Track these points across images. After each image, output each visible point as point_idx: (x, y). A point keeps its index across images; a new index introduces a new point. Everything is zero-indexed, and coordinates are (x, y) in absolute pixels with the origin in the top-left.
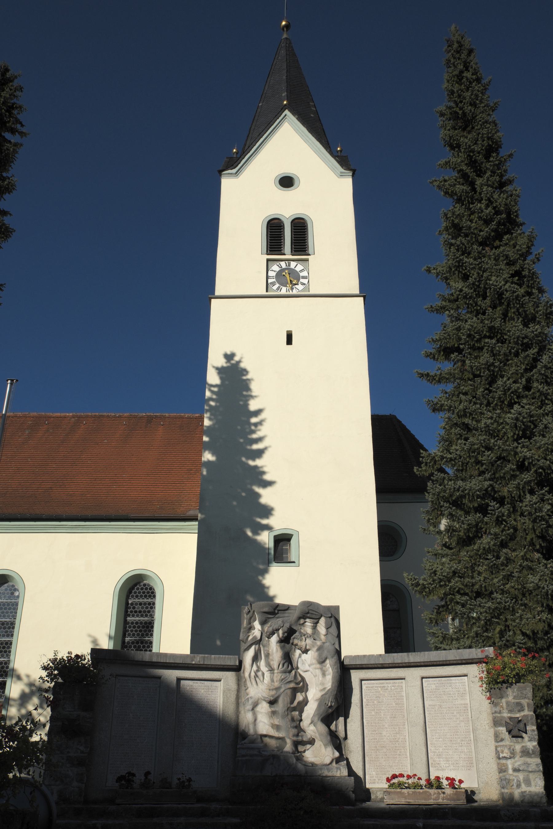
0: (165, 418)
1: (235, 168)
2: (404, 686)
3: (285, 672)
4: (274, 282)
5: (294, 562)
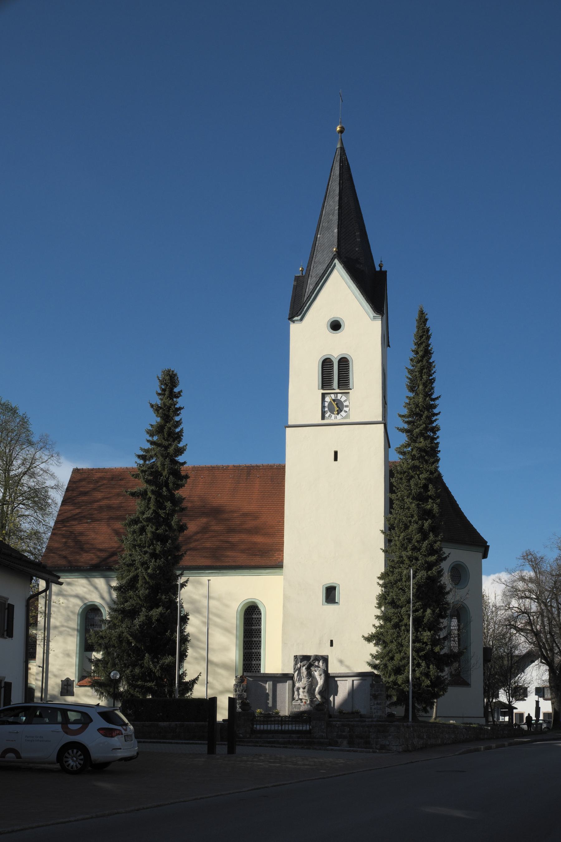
0: (260, 469)
1: (299, 315)
4: (330, 415)
5: (338, 603)
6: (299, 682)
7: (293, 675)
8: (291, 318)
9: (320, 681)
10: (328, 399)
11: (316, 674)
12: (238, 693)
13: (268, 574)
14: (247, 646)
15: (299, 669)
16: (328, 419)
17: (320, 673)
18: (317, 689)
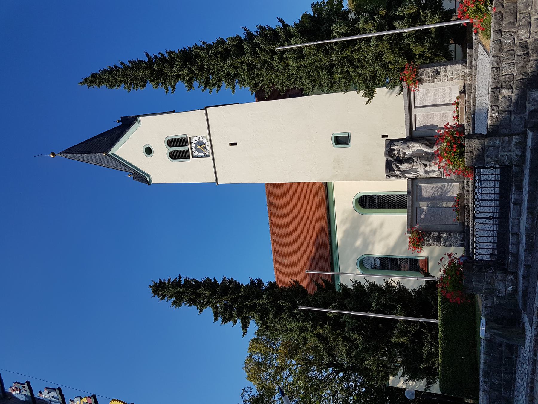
1: (146, 177)
2: (418, 114)
3: (413, 162)
6: (418, 171)
7: (409, 178)
8: (149, 183)
9: (416, 147)
10: (196, 153)
11: (408, 152)
12: (432, 242)
13: (332, 190)
14: (392, 206)
15: (402, 172)
16: (209, 153)
17: (407, 147)
18: (427, 150)
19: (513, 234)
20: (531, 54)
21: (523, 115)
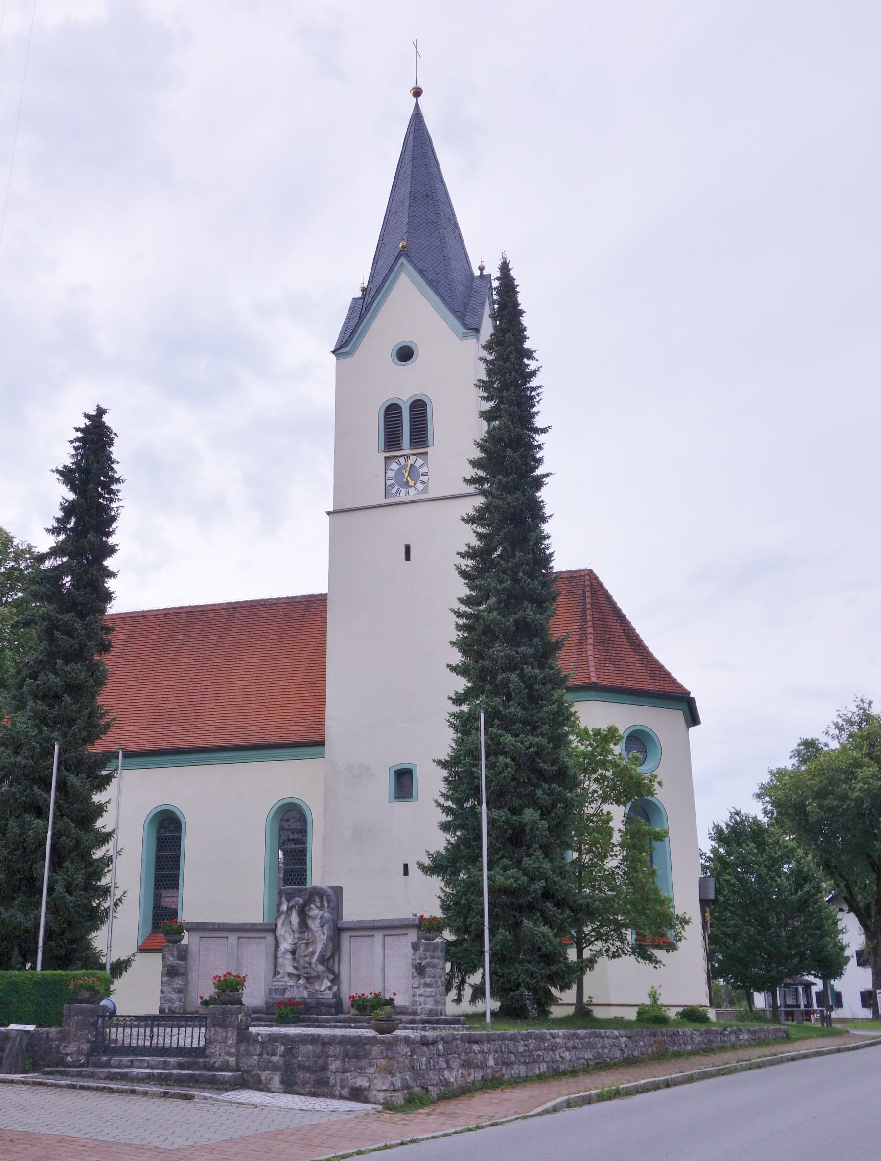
4: (393, 484)
19: (132, 1061)
20: (316, 1075)
21: (256, 1068)
